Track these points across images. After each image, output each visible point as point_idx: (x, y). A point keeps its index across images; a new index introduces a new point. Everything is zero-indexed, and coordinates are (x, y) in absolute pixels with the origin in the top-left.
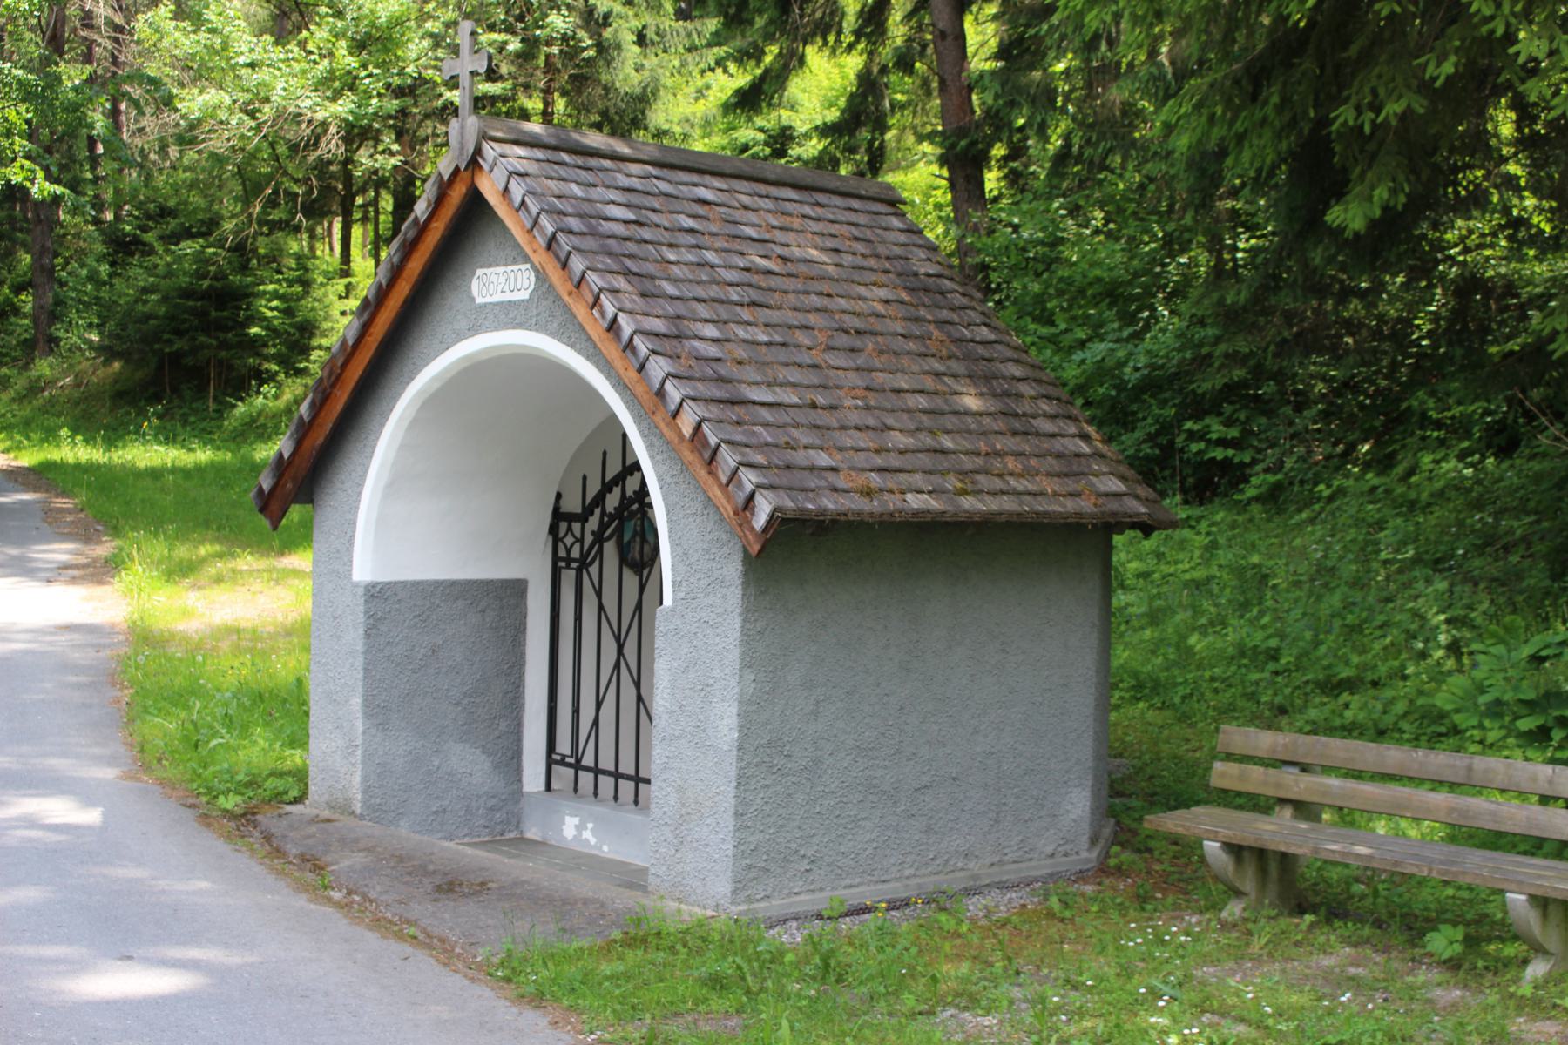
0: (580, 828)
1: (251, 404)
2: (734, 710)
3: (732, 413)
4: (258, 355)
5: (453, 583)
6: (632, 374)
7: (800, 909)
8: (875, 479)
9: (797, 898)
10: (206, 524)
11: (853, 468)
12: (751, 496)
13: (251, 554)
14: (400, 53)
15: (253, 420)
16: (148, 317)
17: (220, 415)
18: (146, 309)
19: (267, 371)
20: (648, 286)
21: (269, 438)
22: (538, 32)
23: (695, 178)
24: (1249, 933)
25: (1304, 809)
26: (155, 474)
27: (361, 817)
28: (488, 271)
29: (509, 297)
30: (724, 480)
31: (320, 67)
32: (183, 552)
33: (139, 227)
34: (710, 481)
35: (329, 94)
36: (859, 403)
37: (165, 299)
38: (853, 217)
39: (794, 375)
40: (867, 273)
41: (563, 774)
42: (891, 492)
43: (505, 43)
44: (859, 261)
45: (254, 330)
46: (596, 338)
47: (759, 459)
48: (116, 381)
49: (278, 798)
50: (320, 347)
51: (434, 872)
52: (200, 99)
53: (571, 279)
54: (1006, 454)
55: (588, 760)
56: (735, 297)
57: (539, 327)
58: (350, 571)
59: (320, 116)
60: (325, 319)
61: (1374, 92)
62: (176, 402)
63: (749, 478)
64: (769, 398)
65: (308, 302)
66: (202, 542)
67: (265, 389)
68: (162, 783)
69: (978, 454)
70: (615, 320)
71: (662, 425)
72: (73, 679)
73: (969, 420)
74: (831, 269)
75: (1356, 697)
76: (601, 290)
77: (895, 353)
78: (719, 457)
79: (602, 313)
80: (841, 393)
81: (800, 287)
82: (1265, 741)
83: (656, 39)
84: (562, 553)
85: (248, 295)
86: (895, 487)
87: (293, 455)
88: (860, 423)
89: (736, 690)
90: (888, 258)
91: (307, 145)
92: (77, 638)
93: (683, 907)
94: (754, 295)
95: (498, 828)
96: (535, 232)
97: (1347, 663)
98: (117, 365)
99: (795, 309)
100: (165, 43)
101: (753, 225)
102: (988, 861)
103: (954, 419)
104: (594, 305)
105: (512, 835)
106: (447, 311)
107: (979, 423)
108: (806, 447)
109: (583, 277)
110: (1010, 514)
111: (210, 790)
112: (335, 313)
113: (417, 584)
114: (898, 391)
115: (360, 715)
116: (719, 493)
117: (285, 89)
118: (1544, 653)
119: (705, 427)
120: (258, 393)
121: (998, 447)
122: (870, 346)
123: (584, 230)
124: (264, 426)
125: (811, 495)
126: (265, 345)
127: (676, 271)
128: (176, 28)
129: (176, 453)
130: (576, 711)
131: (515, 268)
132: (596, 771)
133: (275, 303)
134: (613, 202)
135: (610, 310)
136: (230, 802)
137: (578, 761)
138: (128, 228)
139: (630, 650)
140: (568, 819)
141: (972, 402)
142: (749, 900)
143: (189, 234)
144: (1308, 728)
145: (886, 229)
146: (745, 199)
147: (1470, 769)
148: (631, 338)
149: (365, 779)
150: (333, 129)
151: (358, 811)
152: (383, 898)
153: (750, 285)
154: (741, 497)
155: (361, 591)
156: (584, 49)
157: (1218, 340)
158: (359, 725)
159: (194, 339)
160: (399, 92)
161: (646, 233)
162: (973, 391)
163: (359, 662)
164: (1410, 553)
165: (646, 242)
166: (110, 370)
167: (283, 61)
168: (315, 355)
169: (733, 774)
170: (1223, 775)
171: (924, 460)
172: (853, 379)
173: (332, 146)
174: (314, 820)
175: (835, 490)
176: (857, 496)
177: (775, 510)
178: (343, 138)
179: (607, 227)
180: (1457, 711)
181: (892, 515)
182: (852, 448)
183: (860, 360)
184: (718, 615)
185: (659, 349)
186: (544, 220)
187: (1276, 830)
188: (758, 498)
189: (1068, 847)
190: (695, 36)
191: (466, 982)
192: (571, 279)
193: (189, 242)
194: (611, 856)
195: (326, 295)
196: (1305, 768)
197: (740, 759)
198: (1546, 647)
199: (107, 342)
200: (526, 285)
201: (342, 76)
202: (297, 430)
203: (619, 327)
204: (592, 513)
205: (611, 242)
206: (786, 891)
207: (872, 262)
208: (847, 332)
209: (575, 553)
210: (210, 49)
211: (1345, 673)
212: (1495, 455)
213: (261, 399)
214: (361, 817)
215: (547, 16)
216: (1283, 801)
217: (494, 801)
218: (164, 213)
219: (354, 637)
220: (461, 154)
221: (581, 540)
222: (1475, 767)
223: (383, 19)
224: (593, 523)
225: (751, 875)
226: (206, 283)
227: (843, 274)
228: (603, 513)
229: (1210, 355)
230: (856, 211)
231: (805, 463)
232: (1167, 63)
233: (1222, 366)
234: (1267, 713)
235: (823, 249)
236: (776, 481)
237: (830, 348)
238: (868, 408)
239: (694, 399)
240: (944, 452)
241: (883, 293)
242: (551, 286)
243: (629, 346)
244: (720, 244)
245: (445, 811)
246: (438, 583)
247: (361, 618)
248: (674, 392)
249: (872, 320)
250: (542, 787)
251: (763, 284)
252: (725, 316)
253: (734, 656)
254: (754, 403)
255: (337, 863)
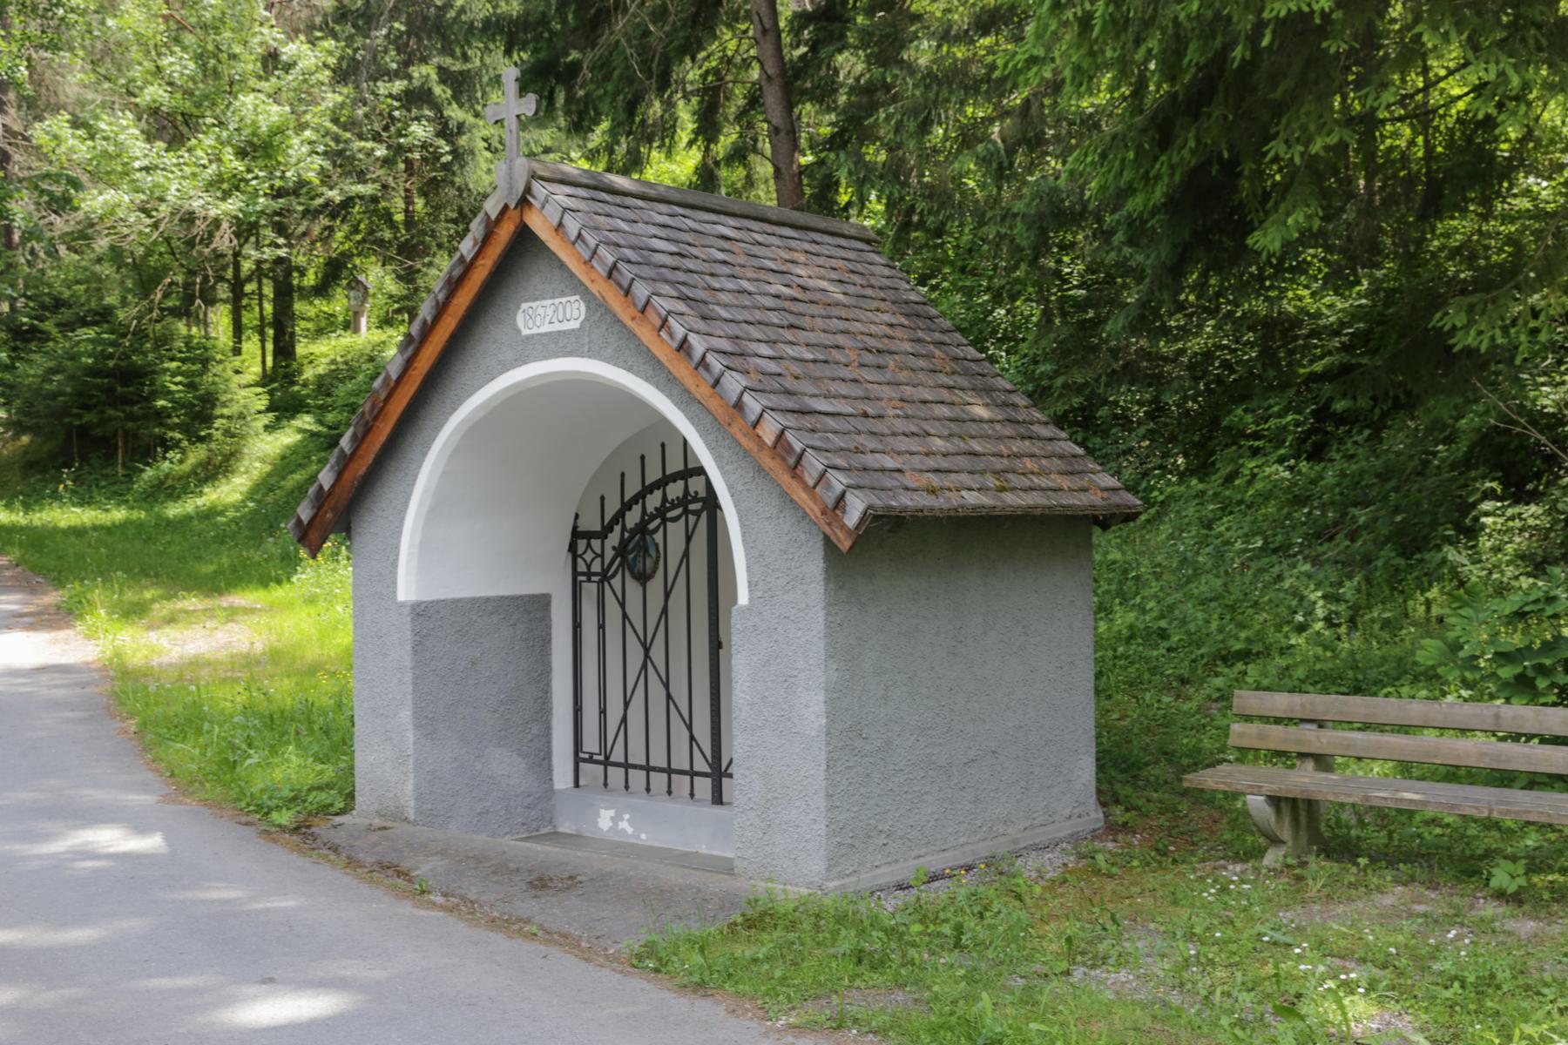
0: (615, 820)
1: (158, 468)
2: (821, 698)
3: (808, 422)
4: (161, 425)
5: (488, 600)
6: (703, 391)
7: (882, 881)
8: (935, 480)
9: (879, 871)
10: (144, 572)
11: (914, 470)
12: (842, 497)
13: (195, 596)
14: (280, 159)
15: (162, 483)
16: (54, 396)
17: (129, 478)
18: (54, 386)
19: (172, 439)
20: (705, 310)
21: (179, 497)
22: (402, 140)
23: (713, 217)
24: (1300, 878)
25: (1322, 761)
26: (78, 532)
27: (415, 823)
28: (534, 305)
29: (557, 327)
30: (811, 482)
31: (210, 171)
32: (130, 596)
33: (36, 318)
34: (794, 484)
35: (219, 194)
36: (899, 412)
37: (72, 378)
38: (844, 253)
39: (843, 389)
40: (869, 301)
41: (591, 771)
42: (950, 490)
43: (373, 150)
44: (860, 290)
45: (161, 403)
46: (663, 359)
47: (840, 462)
48: (26, 453)
49: (325, 810)
50: (222, 416)
51: (518, 870)
52: (101, 198)
53: (635, 305)
54: (1022, 456)
55: (617, 756)
56: (776, 321)
57: (591, 354)
58: (395, 592)
59: (213, 212)
60: (225, 392)
61: (1304, 129)
62: (86, 469)
63: (838, 481)
64: (830, 409)
65: (208, 378)
66: (146, 588)
67: (170, 454)
68: (205, 803)
69: (1002, 456)
70: (685, 340)
71: (739, 436)
72: (70, 715)
73: (986, 426)
74: (841, 297)
75: (1250, 666)
76: (669, 313)
77: (913, 370)
78: (803, 462)
79: (671, 335)
80: (883, 404)
81: (822, 312)
82: (1281, 702)
83: (500, 147)
84: (582, 567)
85: (154, 372)
86: (951, 486)
87: (333, 486)
88: (906, 430)
89: (822, 679)
90: (881, 288)
91: (202, 240)
92: (58, 679)
93: (788, 887)
94: (792, 319)
95: (534, 825)
96: (594, 262)
97: (1237, 639)
98: (25, 439)
99: (825, 331)
100: (63, 149)
101: (770, 259)
102: (1022, 826)
103: (974, 426)
104: (662, 327)
105: (546, 830)
106: (491, 340)
107: (993, 429)
108: (872, 452)
109: (648, 302)
110: (1044, 508)
111: (260, 807)
112: (233, 386)
113: (456, 601)
114: (925, 402)
115: (410, 727)
116: (804, 496)
117: (178, 190)
118: (1527, 609)
119: (789, 435)
120: (165, 458)
121: (1015, 449)
122: (892, 363)
123: (640, 260)
124: (173, 488)
125: (890, 493)
126: (169, 416)
127: (723, 297)
128: (73, 135)
129: (93, 513)
130: (603, 712)
131: (564, 300)
132: (626, 766)
133: (179, 379)
134: (655, 237)
135: (680, 332)
136: (284, 818)
137: (607, 758)
138: (25, 320)
139: (657, 653)
140: (602, 812)
141: (981, 411)
142: (841, 876)
143: (84, 323)
144: (1216, 695)
145: (871, 264)
146: (759, 238)
147: (1497, 717)
148: (704, 357)
149: (417, 786)
150: (225, 225)
151: (412, 817)
152: (484, 898)
153: (785, 310)
154: (830, 500)
155: (407, 610)
156: (442, 155)
157: (1056, 374)
158: (410, 736)
159: (102, 412)
160: (278, 194)
161: (689, 264)
162: (979, 401)
163: (408, 677)
164: (1259, 544)
165: (691, 271)
166: (19, 444)
167: (175, 165)
168: (218, 423)
169: (822, 757)
170: (1241, 735)
171: (963, 462)
172: (887, 392)
173: (224, 241)
174: (370, 829)
175: (907, 489)
176: (925, 494)
177: (869, 507)
178: (234, 233)
179: (658, 258)
180: (1440, 665)
181: (956, 510)
182: (907, 452)
183: (888, 376)
184: (800, 610)
185: (731, 365)
186: (603, 251)
187: (1303, 780)
188: (849, 497)
189: (1080, 809)
190: (533, 144)
191: (619, 976)
192: (635, 305)
193: (85, 330)
194: (649, 843)
195: (224, 370)
196: (1321, 724)
197: (828, 744)
198: (1527, 604)
199: (14, 418)
200: (576, 314)
201: (229, 179)
202: (338, 462)
203: (690, 347)
204: (611, 530)
205: (663, 270)
206: (868, 865)
207: (869, 292)
208: (870, 352)
209: (596, 567)
210: (105, 154)
211: (1238, 646)
212: (1308, 459)
213: (167, 464)
214: (415, 823)
215: (409, 126)
216: (1302, 756)
217: (529, 800)
218: (58, 304)
219: (401, 653)
220: (510, 193)
221: (602, 556)
222: (1502, 714)
223: (264, 129)
224: (614, 539)
225: (841, 852)
226: (111, 363)
227: (853, 301)
228: (624, 528)
229: (1050, 387)
230: (844, 248)
231: (877, 466)
232: (999, 141)
233: (1061, 395)
234: (1175, 684)
235: (831, 280)
236: (861, 482)
237: (862, 365)
238: (907, 417)
239: (772, 410)
240: (975, 454)
241: (887, 318)
242: (609, 311)
243: (703, 363)
244: (750, 274)
245: (487, 812)
246: (474, 601)
247: (409, 635)
248: (753, 405)
249: (886, 341)
250: (571, 784)
251: (795, 310)
252: (773, 337)
253: (818, 647)
254: (820, 413)
255: (418, 868)
